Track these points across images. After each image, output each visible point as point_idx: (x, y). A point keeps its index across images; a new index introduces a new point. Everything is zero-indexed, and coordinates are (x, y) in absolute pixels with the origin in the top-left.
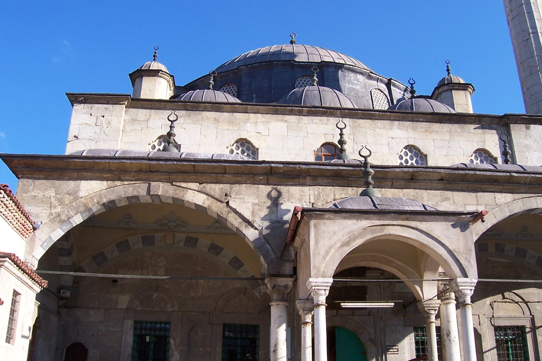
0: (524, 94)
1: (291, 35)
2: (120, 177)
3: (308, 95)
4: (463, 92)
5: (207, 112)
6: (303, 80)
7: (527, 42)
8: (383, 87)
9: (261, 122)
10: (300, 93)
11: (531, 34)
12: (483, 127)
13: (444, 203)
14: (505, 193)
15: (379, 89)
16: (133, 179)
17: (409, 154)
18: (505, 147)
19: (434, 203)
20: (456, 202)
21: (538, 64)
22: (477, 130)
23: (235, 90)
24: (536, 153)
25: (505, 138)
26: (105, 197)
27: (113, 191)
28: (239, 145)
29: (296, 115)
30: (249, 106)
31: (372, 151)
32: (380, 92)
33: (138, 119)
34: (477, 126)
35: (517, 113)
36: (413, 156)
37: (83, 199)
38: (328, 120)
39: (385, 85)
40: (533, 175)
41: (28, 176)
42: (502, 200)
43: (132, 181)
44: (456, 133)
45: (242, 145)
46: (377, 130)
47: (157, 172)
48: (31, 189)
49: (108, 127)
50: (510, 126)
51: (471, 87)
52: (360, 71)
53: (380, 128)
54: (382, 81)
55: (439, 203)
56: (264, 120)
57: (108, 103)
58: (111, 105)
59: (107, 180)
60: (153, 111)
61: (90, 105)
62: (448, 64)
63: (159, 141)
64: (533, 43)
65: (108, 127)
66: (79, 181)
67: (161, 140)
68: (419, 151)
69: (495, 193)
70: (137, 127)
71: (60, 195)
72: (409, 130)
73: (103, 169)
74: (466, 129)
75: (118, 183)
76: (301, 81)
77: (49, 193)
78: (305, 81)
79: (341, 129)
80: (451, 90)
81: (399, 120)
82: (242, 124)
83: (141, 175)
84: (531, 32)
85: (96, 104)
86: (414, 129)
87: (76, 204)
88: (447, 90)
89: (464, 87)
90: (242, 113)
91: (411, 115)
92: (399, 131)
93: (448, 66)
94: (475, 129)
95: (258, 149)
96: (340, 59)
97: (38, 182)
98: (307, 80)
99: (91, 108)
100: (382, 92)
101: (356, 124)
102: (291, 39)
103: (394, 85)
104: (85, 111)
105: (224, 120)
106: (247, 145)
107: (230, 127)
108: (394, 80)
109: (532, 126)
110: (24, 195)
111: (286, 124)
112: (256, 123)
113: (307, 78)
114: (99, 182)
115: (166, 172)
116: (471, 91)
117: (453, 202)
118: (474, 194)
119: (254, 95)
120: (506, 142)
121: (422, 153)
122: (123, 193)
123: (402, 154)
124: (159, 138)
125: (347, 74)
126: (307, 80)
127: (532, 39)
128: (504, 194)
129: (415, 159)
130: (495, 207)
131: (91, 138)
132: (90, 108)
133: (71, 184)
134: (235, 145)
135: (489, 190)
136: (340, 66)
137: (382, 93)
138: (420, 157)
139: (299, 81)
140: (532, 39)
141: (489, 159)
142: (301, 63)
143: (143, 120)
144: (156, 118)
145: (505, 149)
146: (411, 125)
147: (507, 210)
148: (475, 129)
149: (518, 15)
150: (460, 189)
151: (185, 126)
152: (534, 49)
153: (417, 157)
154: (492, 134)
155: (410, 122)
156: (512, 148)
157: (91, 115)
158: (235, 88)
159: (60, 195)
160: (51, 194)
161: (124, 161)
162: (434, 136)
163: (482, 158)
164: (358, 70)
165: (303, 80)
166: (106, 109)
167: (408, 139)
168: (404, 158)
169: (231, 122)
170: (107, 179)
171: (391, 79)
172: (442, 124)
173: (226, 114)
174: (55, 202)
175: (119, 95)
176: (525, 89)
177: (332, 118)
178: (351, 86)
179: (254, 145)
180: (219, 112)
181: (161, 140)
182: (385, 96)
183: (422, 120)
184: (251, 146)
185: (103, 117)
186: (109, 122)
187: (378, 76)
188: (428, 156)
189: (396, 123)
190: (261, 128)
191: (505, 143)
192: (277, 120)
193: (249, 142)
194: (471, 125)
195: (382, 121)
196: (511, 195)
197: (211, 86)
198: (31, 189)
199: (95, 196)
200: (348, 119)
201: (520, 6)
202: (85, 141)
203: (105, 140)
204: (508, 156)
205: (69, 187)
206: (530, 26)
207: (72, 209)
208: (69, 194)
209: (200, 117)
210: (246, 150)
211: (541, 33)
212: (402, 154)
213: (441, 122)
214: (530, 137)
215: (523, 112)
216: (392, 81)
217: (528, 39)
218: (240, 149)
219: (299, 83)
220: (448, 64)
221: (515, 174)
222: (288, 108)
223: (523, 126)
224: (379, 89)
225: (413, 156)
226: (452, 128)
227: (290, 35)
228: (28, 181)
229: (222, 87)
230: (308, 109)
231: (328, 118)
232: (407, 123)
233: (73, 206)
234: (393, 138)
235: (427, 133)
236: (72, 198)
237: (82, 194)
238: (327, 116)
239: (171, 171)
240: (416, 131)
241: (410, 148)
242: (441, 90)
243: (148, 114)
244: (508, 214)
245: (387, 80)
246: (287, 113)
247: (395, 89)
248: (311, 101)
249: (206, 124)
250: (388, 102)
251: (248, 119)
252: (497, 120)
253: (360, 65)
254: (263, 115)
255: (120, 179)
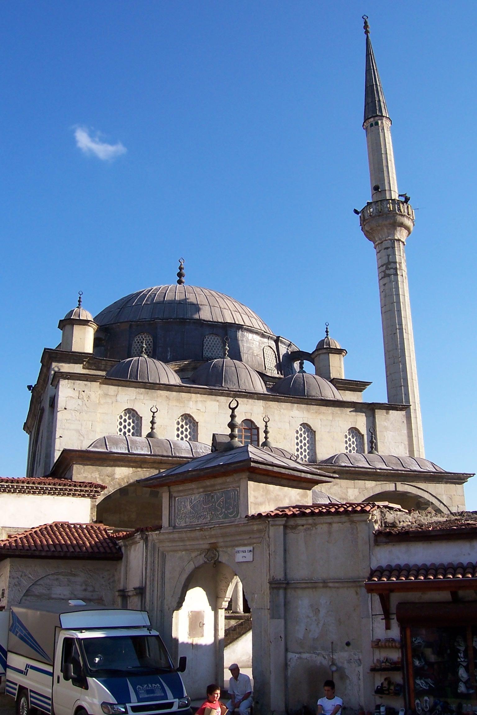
0: (387, 376)
1: (180, 261)
2: (141, 465)
3: (227, 371)
4: (338, 355)
5: (160, 391)
6: (210, 337)
7: (394, 336)
8: (273, 344)
9: (200, 401)
10: (221, 368)
11: (398, 330)
12: (356, 411)
13: (335, 486)
14: (372, 481)
15: (269, 346)
16: (149, 467)
17: (303, 430)
18: (372, 437)
19: (329, 487)
20: (342, 486)
21: (401, 356)
22: (352, 413)
23: (150, 339)
24: (391, 433)
25: (371, 418)
26: (132, 479)
27: (136, 474)
28: (184, 419)
29: (225, 396)
30: (192, 389)
31: (270, 419)
32: (270, 349)
33: (109, 394)
34: (352, 409)
35: (381, 402)
36: (306, 431)
37: (117, 480)
38: (247, 401)
39: (274, 341)
40: (389, 471)
41: (79, 462)
42: (369, 485)
43: (148, 468)
44: (337, 415)
45: (186, 418)
46: (282, 410)
47: (165, 463)
48: (82, 471)
49: (88, 401)
50: (375, 411)
51: (345, 351)
52: (256, 331)
53: (284, 409)
54: (272, 338)
55: (332, 487)
56: (202, 400)
57: (87, 381)
58: (89, 382)
59: (132, 468)
60: (120, 388)
61: (73, 381)
62: (327, 326)
63: (125, 413)
64: (398, 337)
65: (88, 401)
66: (114, 468)
67: (126, 411)
68: (310, 427)
69: (366, 481)
70: (109, 400)
71: (102, 476)
72: (304, 411)
73: (131, 460)
74: (344, 412)
75: (139, 469)
76: (208, 338)
77: (95, 475)
78: (211, 338)
79: (266, 422)
80: (329, 353)
81: (298, 404)
82: (186, 402)
83: (155, 465)
84: (398, 328)
85: (77, 380)
86: (308, 411)
87: (113, 483)
88: (325, 353)
89: (339, 352)
90: (186, 393)
91: (307, 400)
92: (297, 412)
93: (327, 328)
94: (350, 412)
95: (197, 423)
96: (236, 311)
97: (86, 467)
98: (213, 338)
99: (74, 384)
100: (271, 348)
101: (267, 405)
102: (179, 266)
103: (282, 342)
104: (69, 386)
105: (173, 398)
106: (189, 418)
107: (178, 404)
108: (281, 337)
109: (391, 411)
110: (78, 476)
111: (218, 403)
112: (197, 401)
113: (213, 336)
114: (127, 468)
115: (171, 464)
116: (344, 355)
117: (340, 486)
118: (353, 481)
119: (169, 349)
120: (373, 433)
121: (312, 430)
122: (143, 476)
123: (298, 429)
124: (125, 410)
125: (246, 333)
126: (213, 338)
127: (398, 334)
128: (371, 482)
129: (307, 434)
130: (364, 490)
131: (76, 409)
132: (73, 384)
133: (109, 469)
134: (180, 418)
135: (362, 478)
136: (240, 327)
137: (272, 350)
138: (311, 432)
139: (207, 338)
140: (398, 334)
141: (359, 435)
142: (209, 323)
143: (113, 394)
144: (123, 394)
145: (372, 439)
146: (306, 407)
147: (371, 491)
148: (350, 412)
149: (390, 310)
150: (345, 477)
151: (145, 401)
152: (399, 343)
153: (308, 432)
154: (362, 416)
155: (305, 405)
156: (376, 439)
157: (74, 389)
158: (150, 338)
159: (102, 476)
160: (96, 476)
161: (146, 457)
162: (321, 417)
163: (354, 434)
164: (255, 331)
165: (210, 337)
166: (86, 385)
167: (304, 419)
168: (300, 432)
169: (178, 400)
170: (132, 467)
171: (279, 337)
172: (328, 407)
173: (174, 393)
174: (99, 482)
175: (97, 376)
176: (388, 374)
177: (251, 400)
178: (248, 345)
179: (195, 419)
180: (170, 391)
181: (126, 411)
182: (273, 352)
183: (314, 404)
184: (192, 420)
185: (84, 391)
186: (89, 397)
187: (269, 335)
188: (316, 432)
189: (296, 405)
190: (200, 406)
191: (372, 435)
192: (211, 400)
193: (190, 416)
194: (348, 409)
195: (286, 403)
196: (375, 482)
197: (144, 349)
198: (82, 471)
199: (124, 478)
200: (262, 401)
201: (392, 303)
202: (71, 411)
203: (87, 411)
204: (374, 444)
205: (107, 471)
206: (398, 322)
207: (111, 487)
208: (108, 476)
209: (155, 395)
210: (188, 423)
211: (405, 329)
212: (298, 429)
213: (326, 406)
214: (389, 420)
215: (386, 401)
216: (280, 338)
217: (395, 333)
218: (184, 421)
219: (207, 340)
220: (327, 326)
221: (379, 471)
222: (220, 391)
223: (385, 411)
224: (269, 346)
225: (306, 431)
226: (334, 410)
227: (179, 261)
228: (79, 467)
229: (138, 334)
230: (234, 393)
231: (248, 400)
232: (303, 406)
233: (111, 484)
234: (293, 417)
235: (317, 414)
236: (110, 478)
237: (117, 476)
238: (247, 398)
239: (174, 463)
240: (309, 412)
241: (304, 425)
242: (320, 352)
243: (116, 390)
244: (372, 494)
245: (276, 337)
246: (219, 394)
247: (282, 345)
248: (230, 377)
249: (160, 401)
250: (276, 357)
251: (191, 398)
252: (366, 406)
253: (257, 324)
254: (201, 395)
255: (141, 467)
